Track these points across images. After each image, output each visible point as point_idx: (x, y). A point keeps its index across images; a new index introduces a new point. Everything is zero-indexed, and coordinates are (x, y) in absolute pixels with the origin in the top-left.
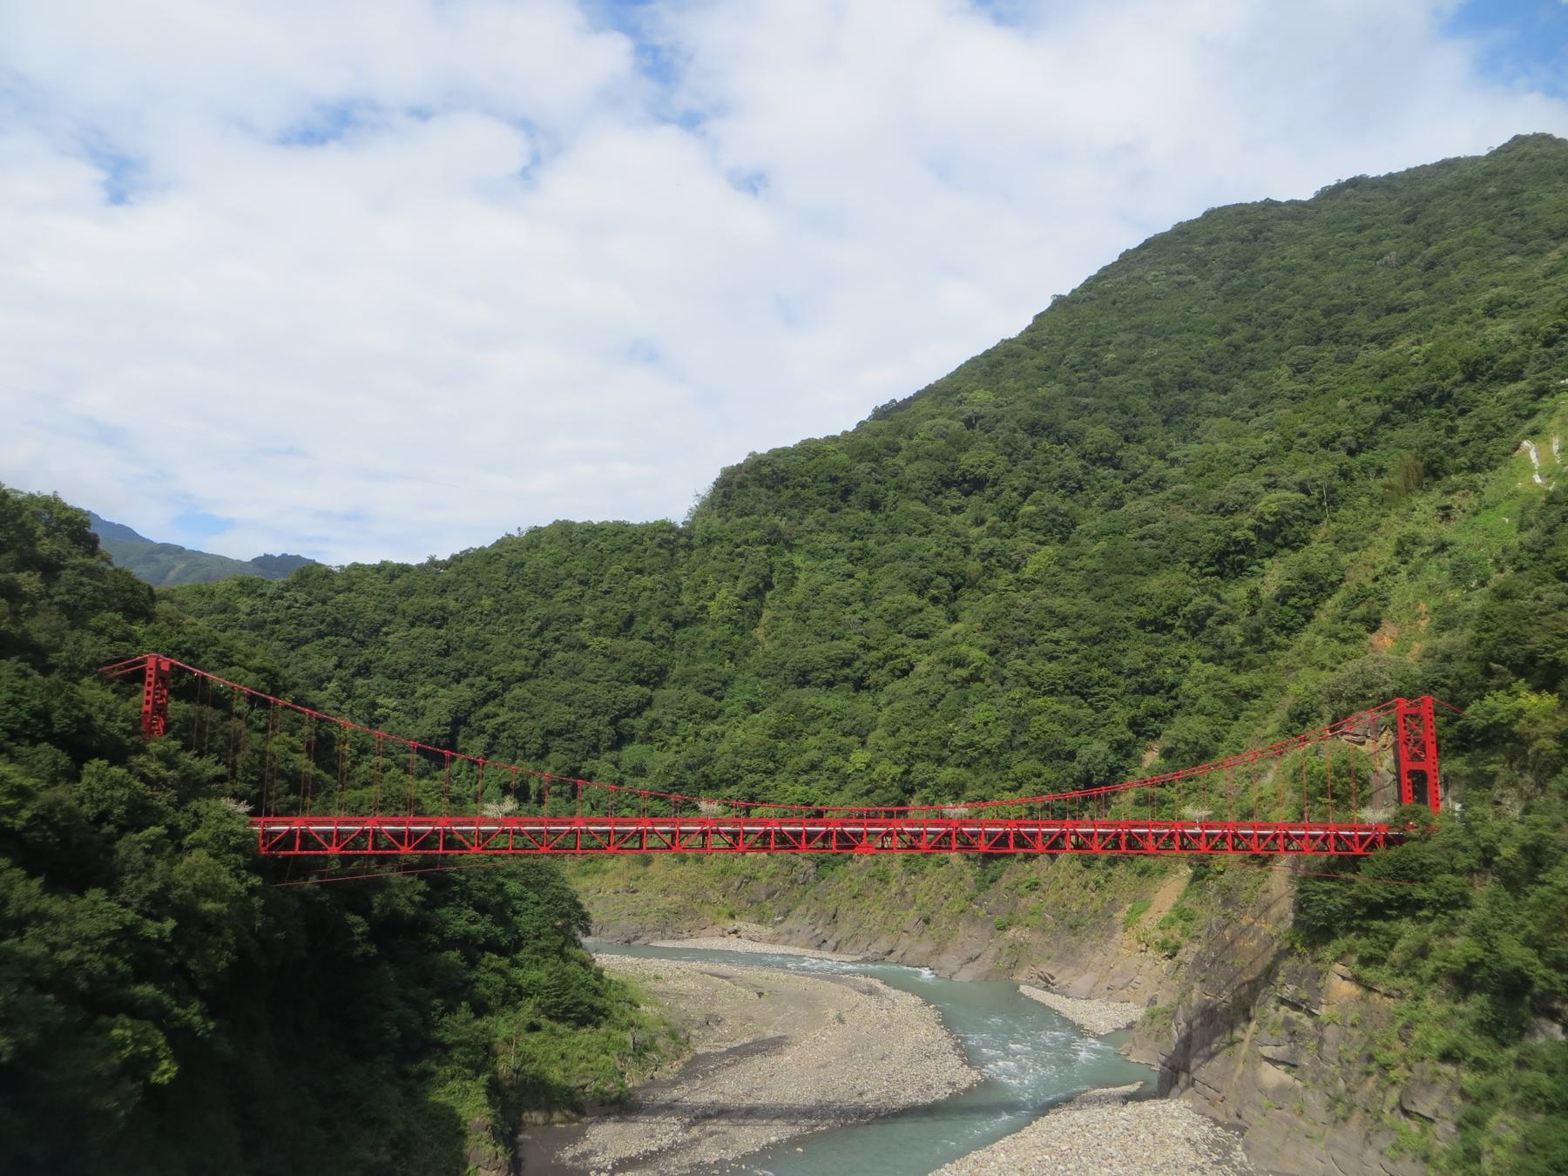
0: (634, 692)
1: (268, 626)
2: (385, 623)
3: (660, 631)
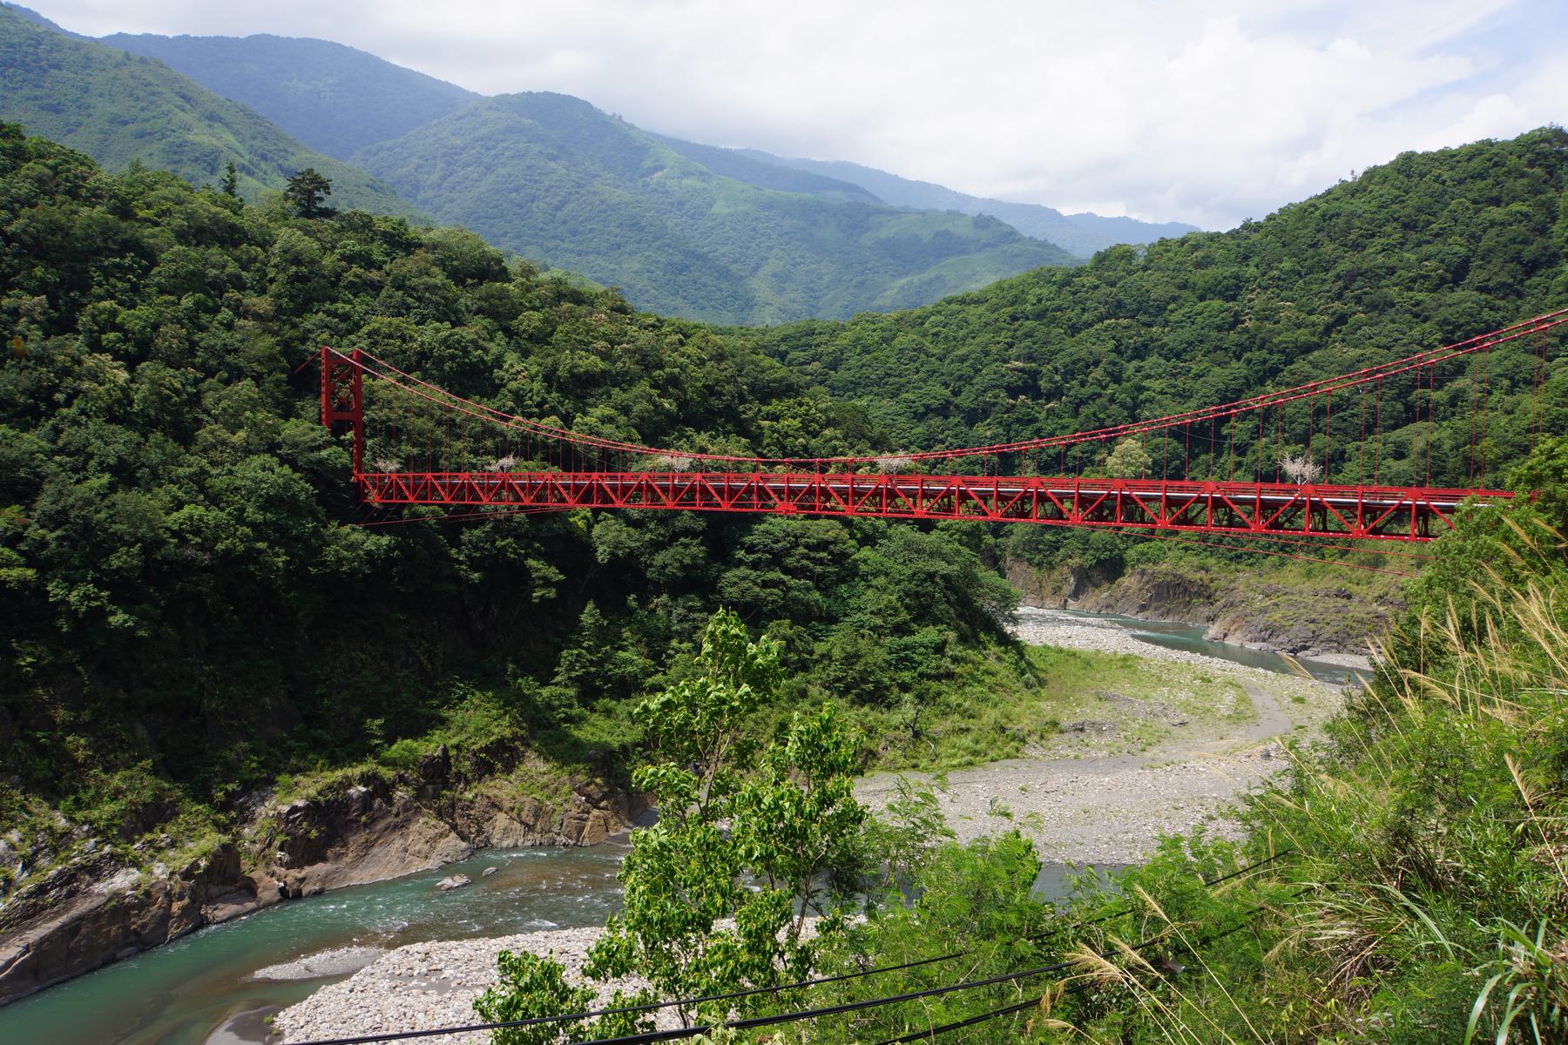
0: (1441, 355)
1: (1049, 314)
2: (1174, 299)
3: (1504, 278)
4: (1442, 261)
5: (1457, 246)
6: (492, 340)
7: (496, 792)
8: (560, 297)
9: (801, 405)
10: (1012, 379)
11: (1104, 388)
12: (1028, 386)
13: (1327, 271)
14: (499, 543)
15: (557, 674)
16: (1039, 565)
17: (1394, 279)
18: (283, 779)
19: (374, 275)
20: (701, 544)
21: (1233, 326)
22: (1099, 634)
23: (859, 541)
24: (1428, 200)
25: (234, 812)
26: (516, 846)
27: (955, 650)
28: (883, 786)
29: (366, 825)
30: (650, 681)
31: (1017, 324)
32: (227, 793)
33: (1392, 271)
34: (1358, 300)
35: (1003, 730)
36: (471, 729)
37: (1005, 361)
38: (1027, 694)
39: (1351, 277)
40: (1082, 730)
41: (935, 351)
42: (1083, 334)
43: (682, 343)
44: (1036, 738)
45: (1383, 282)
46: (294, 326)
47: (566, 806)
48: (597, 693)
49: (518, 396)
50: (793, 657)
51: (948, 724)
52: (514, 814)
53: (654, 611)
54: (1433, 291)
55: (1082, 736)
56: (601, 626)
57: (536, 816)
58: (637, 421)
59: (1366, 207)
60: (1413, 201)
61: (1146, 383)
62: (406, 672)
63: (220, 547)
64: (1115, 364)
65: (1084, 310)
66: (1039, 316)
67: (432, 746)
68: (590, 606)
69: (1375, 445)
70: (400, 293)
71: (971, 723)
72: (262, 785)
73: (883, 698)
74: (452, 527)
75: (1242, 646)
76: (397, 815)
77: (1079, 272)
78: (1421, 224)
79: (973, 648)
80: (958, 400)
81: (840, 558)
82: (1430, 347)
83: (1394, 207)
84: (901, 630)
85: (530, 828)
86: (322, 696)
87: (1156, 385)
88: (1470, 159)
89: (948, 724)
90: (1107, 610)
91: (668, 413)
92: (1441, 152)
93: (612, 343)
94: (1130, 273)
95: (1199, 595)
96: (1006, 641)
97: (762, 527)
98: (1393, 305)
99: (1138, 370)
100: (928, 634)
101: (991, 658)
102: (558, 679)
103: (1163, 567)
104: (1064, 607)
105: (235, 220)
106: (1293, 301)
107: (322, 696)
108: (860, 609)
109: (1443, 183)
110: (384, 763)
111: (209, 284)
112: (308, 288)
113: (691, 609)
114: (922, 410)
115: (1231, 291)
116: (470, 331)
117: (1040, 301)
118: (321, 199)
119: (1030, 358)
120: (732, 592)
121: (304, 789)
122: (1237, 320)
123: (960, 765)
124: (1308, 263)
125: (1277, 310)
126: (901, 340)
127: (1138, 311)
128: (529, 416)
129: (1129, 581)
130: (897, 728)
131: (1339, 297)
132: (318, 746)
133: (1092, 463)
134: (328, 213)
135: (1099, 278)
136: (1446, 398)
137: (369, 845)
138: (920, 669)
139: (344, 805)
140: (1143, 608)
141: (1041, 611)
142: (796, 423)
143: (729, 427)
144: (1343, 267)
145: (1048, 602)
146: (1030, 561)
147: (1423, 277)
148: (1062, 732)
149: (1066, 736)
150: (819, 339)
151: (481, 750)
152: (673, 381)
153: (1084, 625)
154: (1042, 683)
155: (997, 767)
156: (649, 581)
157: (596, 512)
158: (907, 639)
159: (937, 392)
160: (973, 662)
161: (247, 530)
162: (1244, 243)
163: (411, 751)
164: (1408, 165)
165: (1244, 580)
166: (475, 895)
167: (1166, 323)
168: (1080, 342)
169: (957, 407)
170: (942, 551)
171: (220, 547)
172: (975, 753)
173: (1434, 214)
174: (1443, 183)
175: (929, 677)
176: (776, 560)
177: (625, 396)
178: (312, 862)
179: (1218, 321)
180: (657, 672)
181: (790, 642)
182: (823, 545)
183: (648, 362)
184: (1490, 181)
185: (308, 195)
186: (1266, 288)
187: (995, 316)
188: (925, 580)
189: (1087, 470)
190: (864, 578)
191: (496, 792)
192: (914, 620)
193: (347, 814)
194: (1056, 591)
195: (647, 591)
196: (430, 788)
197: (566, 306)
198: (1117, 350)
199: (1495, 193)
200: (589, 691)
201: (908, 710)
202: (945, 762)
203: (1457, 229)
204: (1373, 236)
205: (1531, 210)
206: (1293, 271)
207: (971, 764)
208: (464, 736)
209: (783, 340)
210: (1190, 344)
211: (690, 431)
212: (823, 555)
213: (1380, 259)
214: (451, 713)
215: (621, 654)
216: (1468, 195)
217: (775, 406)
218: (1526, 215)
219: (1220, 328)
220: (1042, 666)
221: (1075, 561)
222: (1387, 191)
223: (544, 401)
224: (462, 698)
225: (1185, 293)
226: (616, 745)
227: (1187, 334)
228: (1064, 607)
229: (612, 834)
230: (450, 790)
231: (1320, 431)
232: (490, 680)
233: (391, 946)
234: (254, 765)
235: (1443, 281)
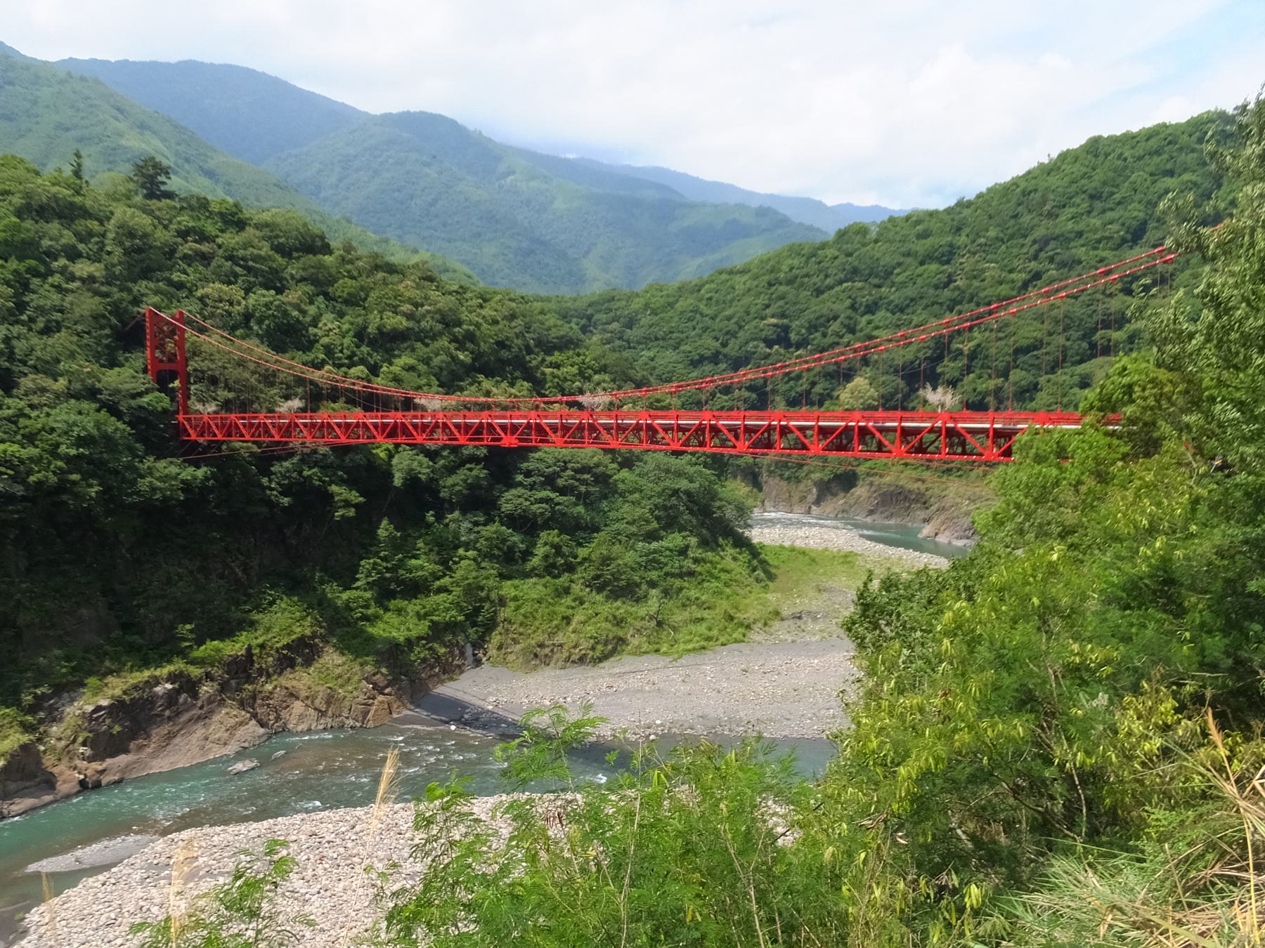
2: (899, 264)
4: (1123, 224)
5: (1135, 211)
6: (311, 303)
7: (294, 683)
8: (377, 268)
9: (578, 355)
10: (770, 333)
11: (841, 337)
12: (782, 338)
13: (1025, 236)
14: (306, 473)
15: (358, 580)
16: (789, 479)
17: (1082, 241)
18: (92, 681)
19: (205, 247)
20: (484, 468)
21: (946, 285)
22: (832, 534)
23: (620, 464)
24: (1111, 174)
25: (41, 713)
26: (309, 730)
27: (695, 553)
28: (627, 669)
29: (169, 718)
30: (438, 583)
31: (773, 288)
32: (36, 696)
33: (1080, 234)
34: (1051, 260)
35: (731, 618)
36: (276, 630)
37: (763, 319)
38: (757, 587)
39: (1045, 242)
40: (800, 618)
41: (708, 312)
42: (826, 295)
43: (481, 307)
44: (760, 625)
45: (1072, 244)
46: (129, 291)
47: (355, 693)
48: (392, 595)
49: (329, 350)
50: (561, 561)
51: (686, 615)
52: (309, 702)
53: (447, 525)
54: (1116, 249)
55: (799, 622)
56: (395, 537)
57: (328, 703)
58: (437, 370)
59: (1060, 183)
60: (1099, 176)
61: (875, 333)
62: (222, 582)
63: (32, 479)
64: (851, 318)
65: (827, 276)
66: (790, 282)
67: (238, 646)
68: (385, 522)
69: (1064, 377)
70: (229, 263)
71: (705, 614)
72: (69, 687)
73: (633, 593)
74: (265, 461)
75: (950, 543)
76: (201, 708)
77: (823, 246)
78: (1105, 195)
79: (713, 550)
80: (726, 350)
81: (603, 479)
82: (1111, 295)
83: (1083, 182)
84: (652, 536)
85: (322, 714)
86: (139, 606)
87: (884, 334)
88: (1147, 140)
89: (686, 615)
90: (843, 516)
91: (462, 363)
92: (1124, 135)
93: (417, 305)
94: (864, 245)
95: (917, 501)
96: (742, 543)
97: (537, 455)
98: (1080, 262)
99: (869, 323)
100: (675, 540)
101: (729, 558)
102: (358, 584)
103: (887, 479)
104: (809, 512)
105: (78, 199)
106: (997, 262)
107: (139, 606)
108: (618, 520)
109: (1125, 159)
110: (193, 662)
111: (44, 253)
112: (144, 260)
113: (476, 524)
114: (697, 357)
115: (947, 255)
116: (293, 295)
117: (791, 269)
118: (164, 183)
119: (783, 315)
120: (506, 507)
121: (116, 687)
122: (950, 280)
123: (694, 649)
124: (1010, 231)
125: (983, 270)
126: (681, 305)
127: (870, 275)
128: (339, 366)
129: (860, 491)
130: (643, 619)
131: (1035, 257)
132: (132, 649)
133: (831, 398)
134: (170, 195)
135: (839, 250)
136: (1125, 337)
137: (170, 736)
138: (667, 569)
139: (152, 701)
140: (871, 512)
141: (790, 515)
142: (575, 370)
143: (517, 374)
144: (1040, 232)
145: (796, 508)
146: (781, 476)
147: (1106, 238)
148: (783, 620)
149: (786, 623)
150: (618, 304)
151: (284, 647)
152: (470, 337)
153: (822, 526)
154: (771, 577)
155: (724, 651)
156: (444, 500)
157: (397, 446)
158: (655, 545)
159: (709, 344)
160: (711, 562)
161: (60, 463)
162: (957, 218)
163: (218, 650)
164: (1095, 147)
165: (954, 489)
166: (263, 778)
167: (893, 284)
168: (823, 302)
169: (725, 356)
170: (691, 473)
171: (32, 479)
172: (709, 639)
173: (1117, 186)
174: (1125, 159)
175: (673, 575)
176: (550, 481)
177: (427, 350)
178: (113, 755)
179: (935, 281)
180: (445, 575)
181: (557, 548)
182: (585, 469)
183: (448, 321)
184: (1165, 156)
185: (151, 179)
186: (974, 254)
187: (756, 283)
188: (671, 496)
189: (827, 403)
190: (622, 495)
191: (294, 683)
192: (664, 528)
193: (151, 709)
194: (802, 499)
195: (442, 508)
196: (233, 682)
197: (380, 275)
198: (853, 307)
199: (1169, 166)
200: (385, 593)
201: (653, 603)
202: (682, 646)
203: (1137, 197)
204: (1064, 206)
205: (1199, 180)
206: (997, 238)
207: (704, 648)
208: (270, 636)
209: (590, 305)
210: (912, 300)
211: (481, 377)
212: (586, 476)
213: (1070, 225)
214: (261, 615)
215: (413, 562)
216: (1147, 169)
217: (557, 357)
218: (1195, 184)
219: (936, 287)
220: (775, 563)
221: (816, 476)
222: (1078, 169)
223: (354, 354)
224: (272, 603)
225: (909, 260)
226: (402, 639)
227: (910, 291)
228: (809, 512)
229: (395, 716)
230: (252, 683)
231: (1017, 367)
232: (296, 586)
233: (165, 832)
234: (64, 670)
235: (1124, 241)
